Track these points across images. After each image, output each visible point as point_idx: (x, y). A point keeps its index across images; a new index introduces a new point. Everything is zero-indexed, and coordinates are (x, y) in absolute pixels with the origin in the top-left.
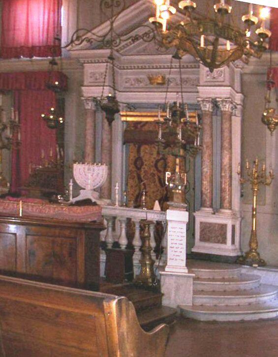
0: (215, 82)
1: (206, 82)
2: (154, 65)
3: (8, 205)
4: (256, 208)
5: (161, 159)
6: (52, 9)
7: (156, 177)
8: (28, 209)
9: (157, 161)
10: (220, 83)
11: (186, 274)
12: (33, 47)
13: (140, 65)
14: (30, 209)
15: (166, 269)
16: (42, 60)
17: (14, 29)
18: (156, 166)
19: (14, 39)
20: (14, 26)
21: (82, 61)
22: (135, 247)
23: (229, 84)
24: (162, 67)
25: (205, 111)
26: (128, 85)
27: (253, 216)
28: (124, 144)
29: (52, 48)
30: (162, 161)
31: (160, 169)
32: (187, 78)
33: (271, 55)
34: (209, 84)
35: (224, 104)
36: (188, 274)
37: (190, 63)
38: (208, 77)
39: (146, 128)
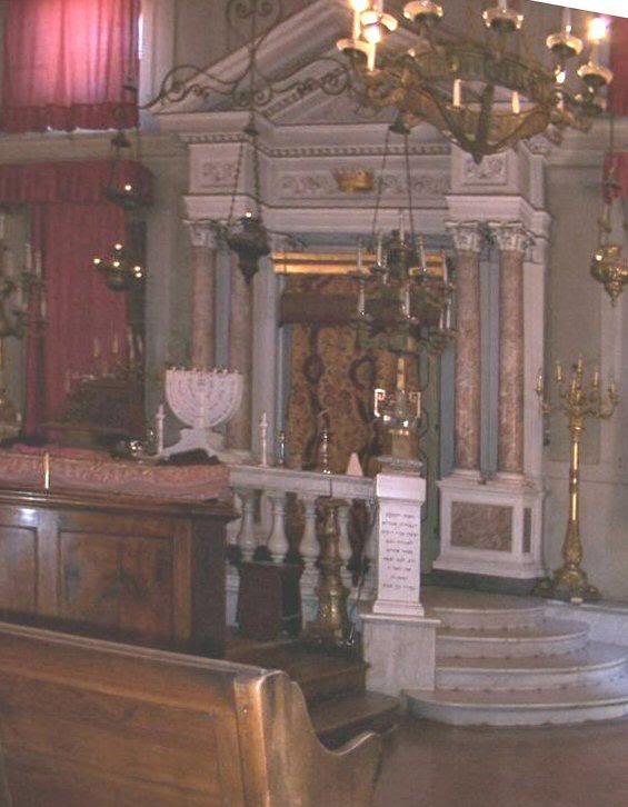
0: (486, 184)
1: (466, 184)
2: (349, 147)
3: (19, 463)
4: (578, 471)
5: (363, 360)
6: (117, 19)
7: (353, 401)
8: (63, 473)
9: (356, 365)
10: (497, 189)
11: (420, 620)
12: (75, 106)
13: (316, 147)
14: (68, 471)
15: (376, 608)
16: (95, 136)
17: (32, 66)
18: (352, 375)
19: (31, 88)
20: (32, 59)
21: (185, 137)
22: (306, 559)
23: (516, 190)
24: (218, 138)
25: (464, 251)
26: (288, 192)
27: (572, 488)
28: (280, 324)
29: (118, 108)
30: (367, 363)
31: (361, 382)
32: (423, 177)
33: (612, 125)
34: (473, 189)
35: (507, 234)
36: (423, 620)
37: (429, 141)
38: (471, 175)
39: (330, 289)
